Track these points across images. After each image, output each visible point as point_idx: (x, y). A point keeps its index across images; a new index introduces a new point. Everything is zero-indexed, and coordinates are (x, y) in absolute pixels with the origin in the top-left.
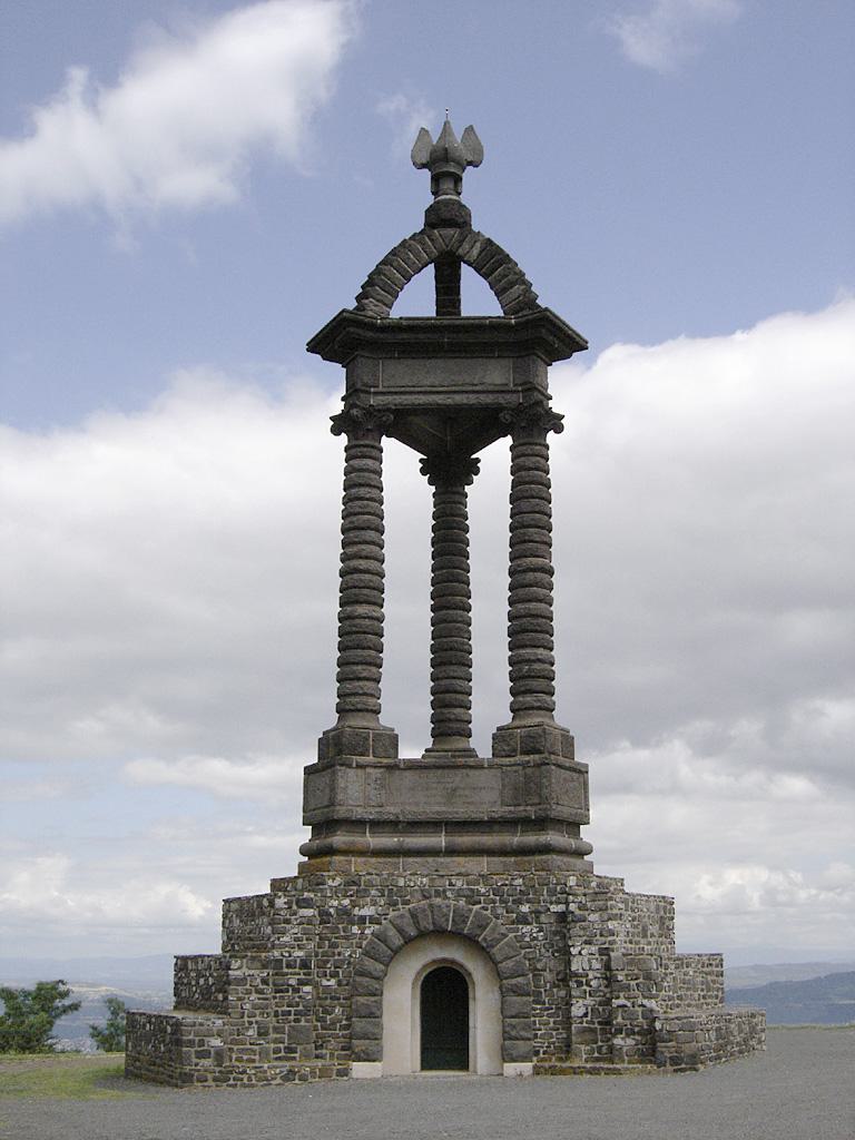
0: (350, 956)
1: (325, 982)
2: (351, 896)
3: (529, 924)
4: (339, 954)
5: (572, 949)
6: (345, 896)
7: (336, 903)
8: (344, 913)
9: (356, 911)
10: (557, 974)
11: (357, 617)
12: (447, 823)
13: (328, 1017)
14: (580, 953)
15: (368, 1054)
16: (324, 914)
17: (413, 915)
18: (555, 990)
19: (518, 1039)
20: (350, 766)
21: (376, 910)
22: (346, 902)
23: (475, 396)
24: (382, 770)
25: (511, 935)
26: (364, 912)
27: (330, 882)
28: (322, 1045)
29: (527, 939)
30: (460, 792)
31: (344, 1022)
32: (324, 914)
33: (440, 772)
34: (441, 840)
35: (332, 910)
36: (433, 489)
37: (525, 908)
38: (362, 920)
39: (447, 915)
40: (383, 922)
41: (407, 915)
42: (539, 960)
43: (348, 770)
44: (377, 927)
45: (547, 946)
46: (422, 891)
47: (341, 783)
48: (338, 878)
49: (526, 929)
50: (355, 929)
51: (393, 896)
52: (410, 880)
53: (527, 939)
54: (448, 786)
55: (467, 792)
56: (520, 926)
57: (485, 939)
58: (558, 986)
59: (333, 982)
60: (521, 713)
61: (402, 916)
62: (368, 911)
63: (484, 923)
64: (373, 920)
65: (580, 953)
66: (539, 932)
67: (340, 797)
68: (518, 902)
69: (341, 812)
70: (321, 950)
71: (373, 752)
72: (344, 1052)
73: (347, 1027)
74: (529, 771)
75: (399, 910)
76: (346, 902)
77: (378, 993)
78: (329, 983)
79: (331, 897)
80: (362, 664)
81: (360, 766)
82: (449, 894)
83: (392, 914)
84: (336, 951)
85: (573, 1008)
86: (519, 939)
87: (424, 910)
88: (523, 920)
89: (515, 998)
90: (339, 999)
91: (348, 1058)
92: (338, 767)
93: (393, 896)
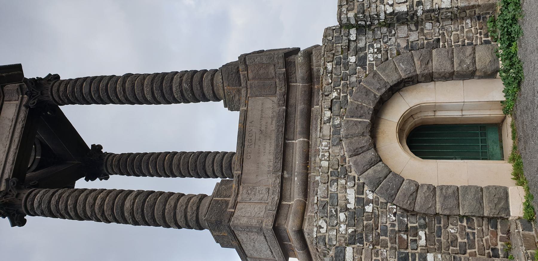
0: (395, 214)
1: (422, 242)
2: (336, 211)
3: (366, 54)
4: (393, 225)
5: (388, 12)
6: (337, 217)
7: (343, 227)
8: (355, 217)
9: (351, 206)
10: (410, 30)
11: (133, 208)
12: (285, 139)
13: (460, 240)
14: (392, 5)
15: (500, 199)
16: (353, 239)
17: (355, 153)
18: (425, 32)
19: (474, 58)
20: (232, 214)
21: (350, 187)
22: (342, 216)
23: (18, 124)
24: (241, 188)
25: (375, 68)
26: (352, 200)
27: (323, 231)
28: (493, 250)
29: (379, 56)
30: (263, 128)
31: (465, 224)
32: (353, 239)
33: (246, 143)
34: (298, 142)
35: (350, 230)
36: (98, 179)
37: (352, 59)
38: (359, 201)
39: (356, 123)
40: (361, 181)
41: (354, 158)
42: (399, 45)
43: (235, 215)
44: (366, 188)
45: (385, 40)
46: (333, 145)
47: (244, 221)
48: (320, 223)
49: (370, 57)
50: (369, 209)
51: (339, 172)
52: (323, 156)
53: (379, 56)
54: (257, 137)
55: (264, 123)
56: (368, 62)
57: (378, 89)
58: (422, 30)
59: (422, 233)
60: (215, 88)
61: (356, 164)
62: (351, 195)
63: (364, 91)
64: (360, 191)
65: (392, 5)
66: (373, 47)
67: (254, 222)
68: (347, 65)
69: (268, 224)
70: (389, 245)
71: (227, 197)
72: (499, 227)
73: (469, 218)
74: (251, 76)
75: (350, 167)
76: (342, 216)
77: (433, 189)
78: (423, 237)
79: (338, 231)
80: (165, 205)
81: (235, 206)
82: (337, 122)
83: (353, 173)
84: (390, 228)
85: (443, 6)
86: (379, 62)
87: (351, 143)
88: (362, 62)
89: (434, 63)
90: (440, 228)
91: (505, 220)
92: (231, 223)
93: (339, 172)
